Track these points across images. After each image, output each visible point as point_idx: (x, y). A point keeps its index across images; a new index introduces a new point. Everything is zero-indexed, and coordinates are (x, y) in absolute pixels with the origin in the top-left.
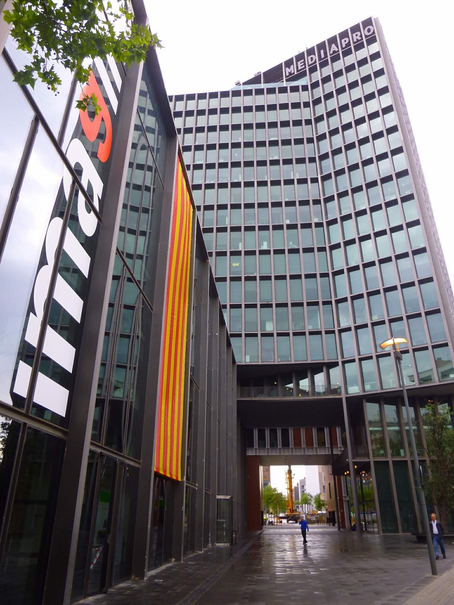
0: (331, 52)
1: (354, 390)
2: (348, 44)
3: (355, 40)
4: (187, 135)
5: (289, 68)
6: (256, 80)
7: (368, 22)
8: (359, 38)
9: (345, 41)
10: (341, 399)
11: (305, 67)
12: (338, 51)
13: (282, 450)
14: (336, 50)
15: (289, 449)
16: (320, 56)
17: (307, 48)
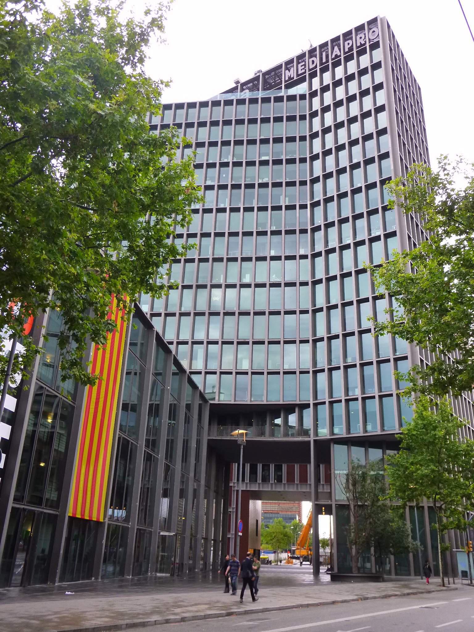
0: (333, 56)
1: (324, 432)
2: (351, 49)
3: (359, 44)
4: (202, 109)
5: (289, 71)
6: (252, 84)
7: (373, 22)
8: (363, 42)
9: (349, 44)
10: (309, 442)
11: (305, 72)
12: (340, 56)
13: (286, 485)
14: (339, 54)
15: (294, 484)
16: (321, 59)
17: (311, 46)
